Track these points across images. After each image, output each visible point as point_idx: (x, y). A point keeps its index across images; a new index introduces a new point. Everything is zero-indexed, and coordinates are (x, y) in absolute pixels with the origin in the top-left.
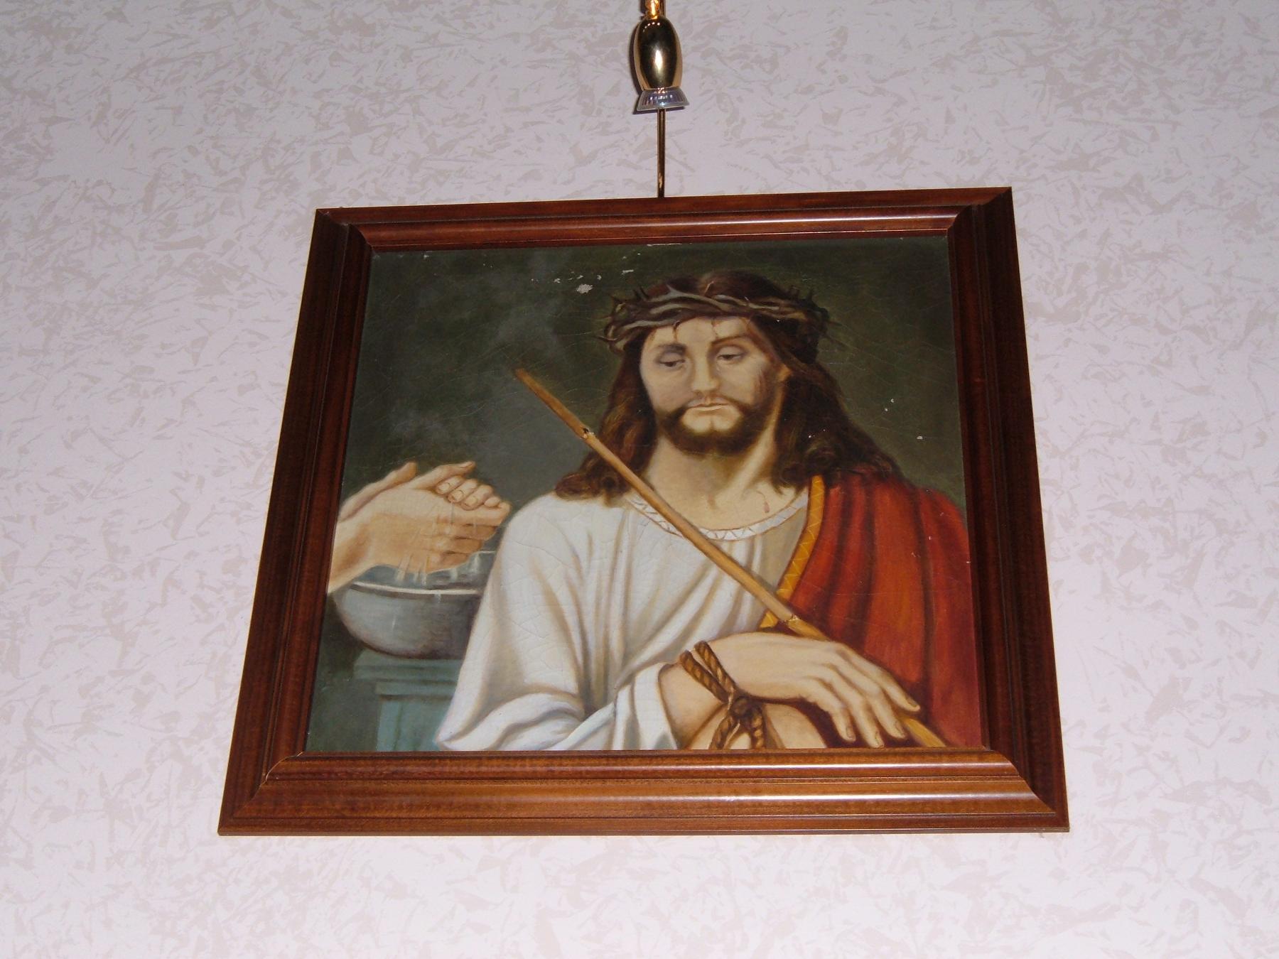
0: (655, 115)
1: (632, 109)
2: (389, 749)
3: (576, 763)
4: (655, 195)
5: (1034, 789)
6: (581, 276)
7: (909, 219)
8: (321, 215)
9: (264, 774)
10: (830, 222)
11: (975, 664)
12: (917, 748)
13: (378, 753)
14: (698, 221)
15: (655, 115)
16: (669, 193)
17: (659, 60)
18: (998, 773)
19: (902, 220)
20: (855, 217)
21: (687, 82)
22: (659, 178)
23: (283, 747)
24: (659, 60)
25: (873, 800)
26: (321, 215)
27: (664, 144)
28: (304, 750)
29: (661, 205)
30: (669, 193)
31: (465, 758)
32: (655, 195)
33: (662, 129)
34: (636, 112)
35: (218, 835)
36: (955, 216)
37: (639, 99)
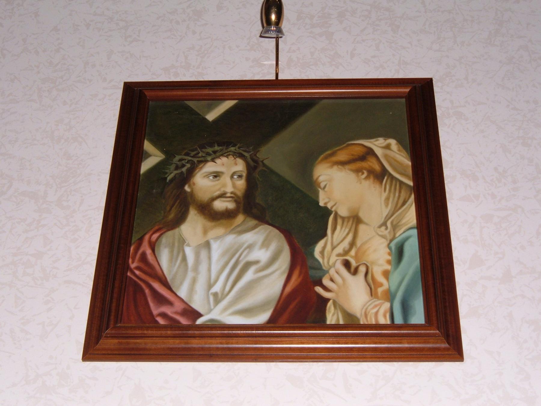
0: (274, 39)
2: (333, 322)
4: (274, 78)
7: (395, 91)
8: (431, 80)
9: (103, 334)
10: (350, 92)
12: (179, 325)
13: (411, 324)
14: (256, 91)
15: (274, 39)
16: (280, 78)
19: (276, 93)
20: (285, 90)
23: (112, 323)
25: (349, 344)
26: (431, 80)
29: (277, 83)
31: (416, 327)
32: (274, 78)
36: (407, 90)
37: (263, 30)
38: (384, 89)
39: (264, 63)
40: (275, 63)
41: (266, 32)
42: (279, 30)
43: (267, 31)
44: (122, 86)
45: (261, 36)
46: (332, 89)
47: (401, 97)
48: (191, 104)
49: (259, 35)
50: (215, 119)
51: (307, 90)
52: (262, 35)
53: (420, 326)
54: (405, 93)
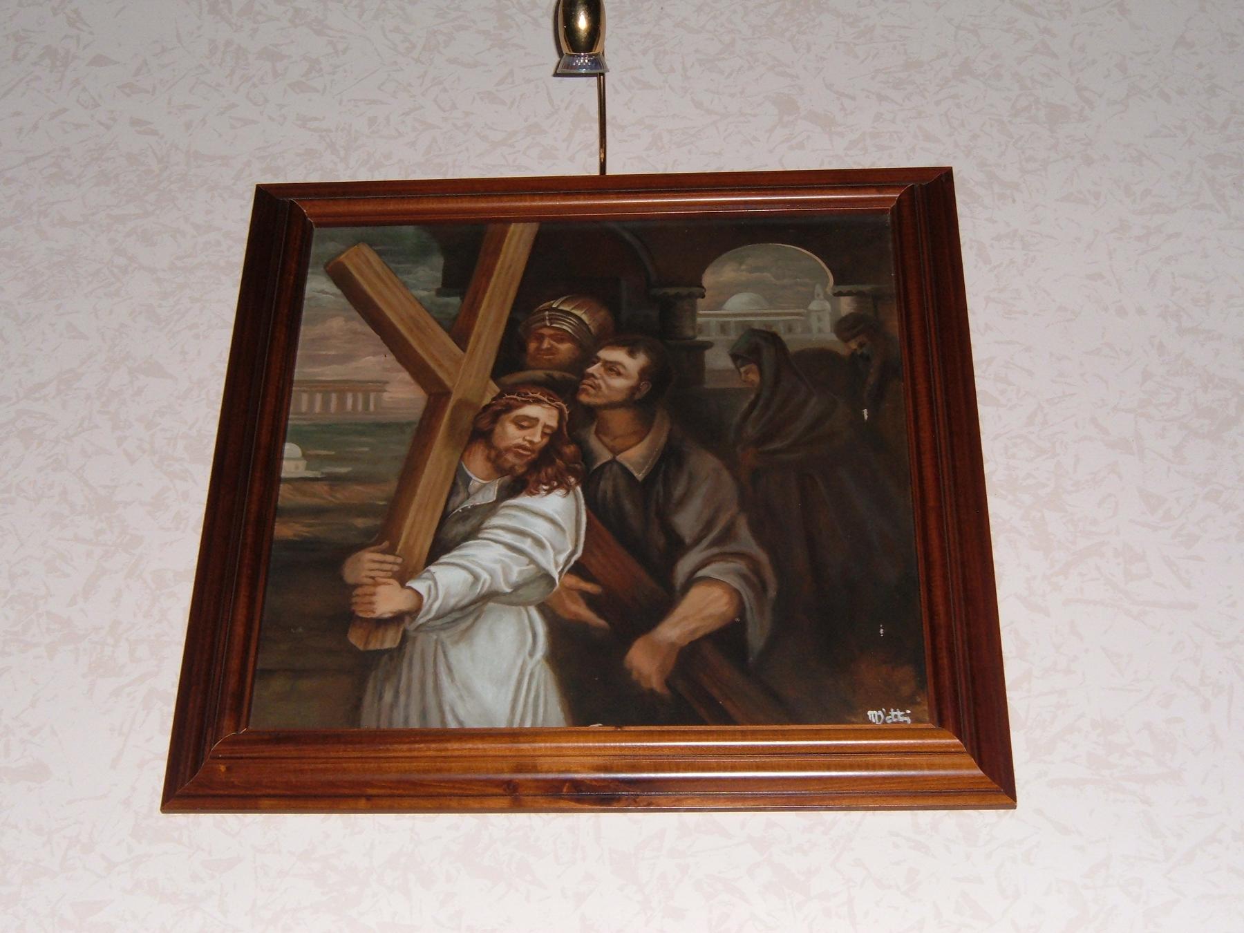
1: (552, 71)
3: (821, 787)
4: (596, 172)
5: (981, 765)
6: (865, 412)
11: (419, 491)
16: (610, 171)
17: (582, 23)
18: (944, 751)
21: (611, 45)
22: (600, 153)
24: (582, 23)
27: (605, 115)
28: (247, 727)
29: (603, 184)
30: (610, 171)
32: (596, 172)
33: (602, 101)
34: (556, 75)
35: (159, 811)
37: (559, 62)
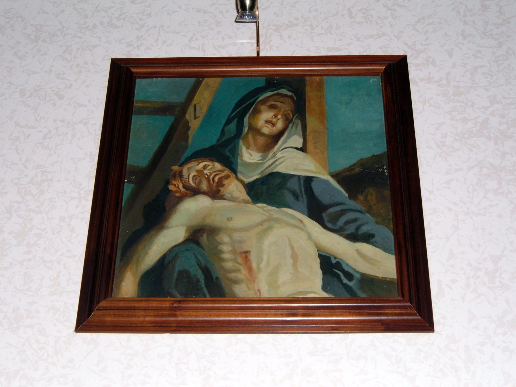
8: (112, 59)
29: (258, 60)
32: (255, 55)
37: (238, 15)
38: (339, 67)
39: (237, 41)
40: (255, 41)
41: (242, 17)
42: (254, 17)
43: (242, 16)
44: (111, 59)
45: (236, 21)
46: (294, 67)
47: (377, 75)
48: (325, 295)
49: (234, 20)
50: (370, 275)
51: (311, 67)
52: (237, 20)
53: (333, 300)
54: (382, 69)
